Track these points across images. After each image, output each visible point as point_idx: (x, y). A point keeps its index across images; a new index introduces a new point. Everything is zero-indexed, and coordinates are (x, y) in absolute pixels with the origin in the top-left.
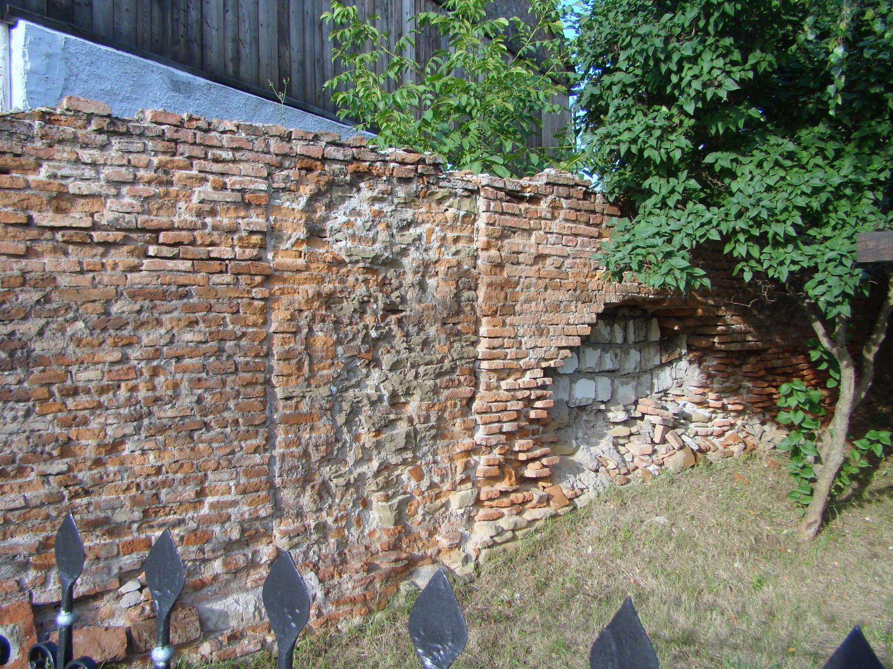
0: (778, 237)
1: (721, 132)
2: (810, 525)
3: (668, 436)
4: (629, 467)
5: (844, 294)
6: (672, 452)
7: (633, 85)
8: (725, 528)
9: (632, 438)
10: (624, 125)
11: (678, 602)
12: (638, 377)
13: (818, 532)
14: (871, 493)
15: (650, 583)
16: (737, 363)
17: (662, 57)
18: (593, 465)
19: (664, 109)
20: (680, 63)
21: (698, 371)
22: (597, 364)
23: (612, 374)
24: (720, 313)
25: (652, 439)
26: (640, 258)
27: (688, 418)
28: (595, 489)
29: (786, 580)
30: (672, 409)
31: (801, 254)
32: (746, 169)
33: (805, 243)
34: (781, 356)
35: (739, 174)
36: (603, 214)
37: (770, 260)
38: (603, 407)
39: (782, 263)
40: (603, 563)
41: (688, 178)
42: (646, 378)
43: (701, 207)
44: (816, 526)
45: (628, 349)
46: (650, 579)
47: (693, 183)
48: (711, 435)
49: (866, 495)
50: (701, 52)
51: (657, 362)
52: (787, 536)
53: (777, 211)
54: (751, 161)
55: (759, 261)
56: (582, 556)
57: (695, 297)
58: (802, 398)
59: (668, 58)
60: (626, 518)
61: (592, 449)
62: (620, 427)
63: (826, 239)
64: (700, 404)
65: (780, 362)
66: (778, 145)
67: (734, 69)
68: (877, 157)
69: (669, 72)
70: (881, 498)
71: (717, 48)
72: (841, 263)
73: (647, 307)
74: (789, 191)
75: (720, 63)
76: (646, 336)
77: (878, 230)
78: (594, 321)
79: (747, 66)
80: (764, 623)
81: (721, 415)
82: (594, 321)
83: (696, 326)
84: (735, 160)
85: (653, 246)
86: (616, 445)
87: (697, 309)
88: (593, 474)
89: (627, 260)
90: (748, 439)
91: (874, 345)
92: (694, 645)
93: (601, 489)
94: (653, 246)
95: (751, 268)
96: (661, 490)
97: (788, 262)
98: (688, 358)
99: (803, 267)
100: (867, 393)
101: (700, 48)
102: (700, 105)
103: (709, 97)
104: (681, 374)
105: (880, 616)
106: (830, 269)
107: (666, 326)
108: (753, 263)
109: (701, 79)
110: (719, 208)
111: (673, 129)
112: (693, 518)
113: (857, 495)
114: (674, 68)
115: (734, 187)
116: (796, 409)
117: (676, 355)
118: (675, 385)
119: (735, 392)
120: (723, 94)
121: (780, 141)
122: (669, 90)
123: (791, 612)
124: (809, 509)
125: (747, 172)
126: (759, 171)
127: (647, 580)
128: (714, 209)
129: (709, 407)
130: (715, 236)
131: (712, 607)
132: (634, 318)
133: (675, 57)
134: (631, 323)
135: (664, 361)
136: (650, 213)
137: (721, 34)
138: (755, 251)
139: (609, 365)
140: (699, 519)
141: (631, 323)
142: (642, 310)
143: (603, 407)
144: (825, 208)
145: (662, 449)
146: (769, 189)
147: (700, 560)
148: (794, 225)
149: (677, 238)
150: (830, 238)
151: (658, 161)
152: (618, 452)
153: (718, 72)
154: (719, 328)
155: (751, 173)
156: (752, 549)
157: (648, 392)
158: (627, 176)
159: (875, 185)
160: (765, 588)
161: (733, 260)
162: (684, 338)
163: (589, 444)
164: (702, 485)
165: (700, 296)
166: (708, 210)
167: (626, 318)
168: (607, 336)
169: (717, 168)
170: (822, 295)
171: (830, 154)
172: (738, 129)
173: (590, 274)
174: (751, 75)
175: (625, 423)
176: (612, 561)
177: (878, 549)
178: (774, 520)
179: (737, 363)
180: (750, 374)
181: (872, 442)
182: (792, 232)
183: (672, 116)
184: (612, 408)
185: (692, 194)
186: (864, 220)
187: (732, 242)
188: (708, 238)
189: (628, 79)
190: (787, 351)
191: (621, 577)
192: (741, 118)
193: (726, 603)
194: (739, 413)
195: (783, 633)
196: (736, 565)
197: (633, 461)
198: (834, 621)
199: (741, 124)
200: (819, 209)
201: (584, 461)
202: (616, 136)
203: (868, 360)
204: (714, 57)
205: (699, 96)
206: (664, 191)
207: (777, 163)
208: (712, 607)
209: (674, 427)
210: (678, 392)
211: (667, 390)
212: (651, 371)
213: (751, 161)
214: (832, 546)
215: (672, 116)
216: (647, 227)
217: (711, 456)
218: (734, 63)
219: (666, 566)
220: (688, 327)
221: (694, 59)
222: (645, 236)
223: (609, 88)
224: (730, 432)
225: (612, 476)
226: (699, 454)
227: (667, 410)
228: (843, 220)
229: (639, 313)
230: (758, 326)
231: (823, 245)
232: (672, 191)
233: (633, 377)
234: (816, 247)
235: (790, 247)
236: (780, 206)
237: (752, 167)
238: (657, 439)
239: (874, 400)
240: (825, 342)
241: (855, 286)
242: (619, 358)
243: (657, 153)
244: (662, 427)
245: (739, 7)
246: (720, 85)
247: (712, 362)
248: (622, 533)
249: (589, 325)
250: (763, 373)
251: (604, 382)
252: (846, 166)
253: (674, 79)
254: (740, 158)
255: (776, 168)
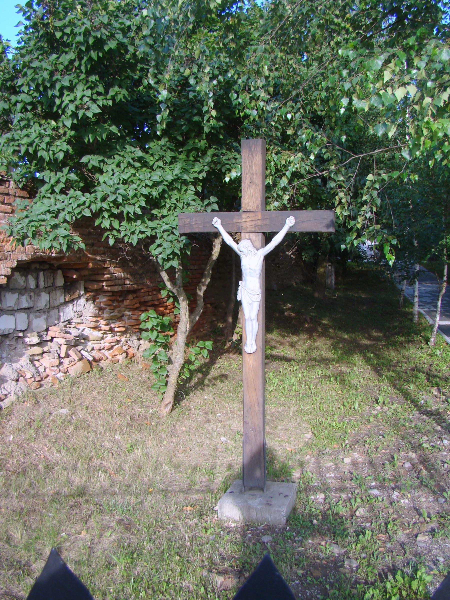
0: (130, 215)
1: (91, 141)
2: (167, 405)
3: (71, 352)
4: (42, 376)
5: (173, 253)
6: (73, 363)
7: (31, 103)
8: (110, 412)
9: (44, 355)
10: (25, 132)
11: (75, 469)
12: (48, 312)
13: (173, 409)
14: (209, 380)
15: (56, 456)
16: (120, 299)
17: (49, 85)
18: (14, 376)
19: (53, 123)
20: (61, 90)
21: (92, 306)
22: (15, 304)
23: (28, 311)
24: (106, 266)
25: (59, 355)
26: (34, 229)
27: (86, 338)
28: (15, 393)
29: (150, 443)
30: (74, 332)
31: (147, 227)
32: (109, 168)
33: (150, 220)
34: (150, 294)
35: (105, 171)
36: (15, 196)
37: (125, 230)
38: (21, 334)
39: (133, 233)
40: (20, 446)
41: (69, 173)
42: (54, 312)
43: (79, 193)
44: (171, 406)
45: (39, 292)
46: (55, 454)
47: (73, 176)
48: (103, 349)
49: (206, 382)
50: (76, 84)
51: (62, 300)
52: (152, 414)
53: (130, 197)
54: (113, 163)
55: (119, 231)
56: (5, 443)
57: (87, 255)
58: (155, 322)
59: (53, 86)
60: (38, 413)
61: (14, 365)
62: (36, 348)
63: (163, 217)
64: (94, 328)
65: (150, 298)
66: (132, 153)
67: (99, 98)
68: (198, 163)
69: (54, 96)
70: (216, 383)
71: (87, 82)
72: (173, 233)
73: (53, 262)
74: (137, 184)
75: (88, 93)
76: (53, 284)
77: (196, 212)
78: (10, 273)
79: (109, 97)
80: (134, 474)
81: (110, 335)
82: (10, 273)
83: (91, 275)
84: (103, 161)
85: (44, 220)
86: (32, 361)
87: (89, 263)
88: (14, 383)
89: (25, 231)
90: (130, 350)
91: (203, 285)
92: (85, 496)
93: (20, 393)
94: (44, 220)
95: (114, 236)
96: (65, 390)
97: (137, 232)
98: (86, 297)
99: (147, 236)
100: (200, 317)
101: (76, 81)
102: (75, 121)
103: (80, 116)
104: (80, 308)
105: (208, 459)
106: (165, 237)
107: (68, 275)
108: (115, 233)
109: (75, 103)
110: (90, 194)
111: (59, 138)
112: (87, 408)
113: (201, 384)
114: (58, 94)
115: (101, 179)
116: (152, 330)
117: (76, 295)
118: (76, 316)
119: (120, 318)
120: (90, 114)
121: (133, 149)
122: (55, 109)
123: (153, 465)
124: (165, 395)
125: (110, 170)
126: (118, 169)
127: (53, 455)
128: (87, 195)
129: (101, 330)
130: (87, 213)
131: (99, 468)
132: (44, 270)
133: (58, 86)
134: (41, 274)
135: (67, 300)
136: (44, 197)
137: (89, 73)
138: (116, 224)
139: (25, 304)
140: (92, 408)
141: (41, 274)
142: (50, 264)
143: (21, 334)
144: (162, 195)
145: (66, 361)
146: (125, 182)
147: (91, 436)
148: (140, 207)
149: (62, 215)
150: (167, 216)
151: (47, 159)
152: (34, 365)
153: (88, 99)
154: (106, 276)
155: (113, 170)
156: (129, 425)
157: (57, 322)
158: (32, 170)
159: (195, 182)
160: (136, 451)
161: (101, 231)
162: (82, 283)
163: (11, 361)
164: (95, 384)
165: (90, 254)
166: (84, 195)
167: (37, 271)
168: (22, 284)
169: (90, 167)
170: (160, 254)
171: (168, 159)
172: (102, 139)
173: (5, 240)
174: (110, 103)
175: (38, 345)
176: (27, 444)
177: (210, 416)
178: (144, 404)
179: (120, 299)
180: (129, 307)
181: (201, 348)
182: (139, 211)
183: (58, 128)
184: (29, 335)
185: (74, 184)
186: (188, 204)
187: (101, 217)
188: (83, 215)
189: (28, 99)
190: (155, 290)
191: (34, 455)
192: (104, 133)
193: (109, 464)
194: (123, 333)
195: (146, 479)
196: (117, 437)
197: (45, 371)
198: (180, 467)
199: (104, 137)
200: (158, 196)
201: (7, 374)
202: (18, 140)
203: (200, 296)
204: (85, 89)
205: (74, 115)
206: (53, 181)
207: (129, 164)
208: (99, 468)
209: (75, 346)
210: (79, 321)
211: (71, 320)
212: (58, 307)
213: (113, 163)
214: (182, 417)
215: (58, 128)
216: (41, 206)
217: (103, 364)
218: (99, 94)
219: (67, 443)
220: (85, 276)
221: (71, 89)
222: (38, 213)
223: (15, 105)
224: (117, 346)
225: (29, 383)
226: (94, 363)
227: (70, 334)
228: (174, 204)
229: (47, 266)
230: (134, 274)
231: (161, 221)
232: (58, 182)
233: (44, 312)
234: (157, 222)
235: (139, 222)
236: (131, 193)
237: (114, 166)
238: (63, 355)
239: (214, 319)
240: (169, 285)
241: (180, 248)
242: (33, 299)
243: (46, 153)
244: (66, 346)
245: (101, 55)
246: (88, 109)
247: (103, 299)
248: (35, 424)
249: (6, 276)
250: (138, 305)
251: (22, 318)
252: (177, 168)
253: (58, 102)
254: (106, 160)
255: (129, 168)
